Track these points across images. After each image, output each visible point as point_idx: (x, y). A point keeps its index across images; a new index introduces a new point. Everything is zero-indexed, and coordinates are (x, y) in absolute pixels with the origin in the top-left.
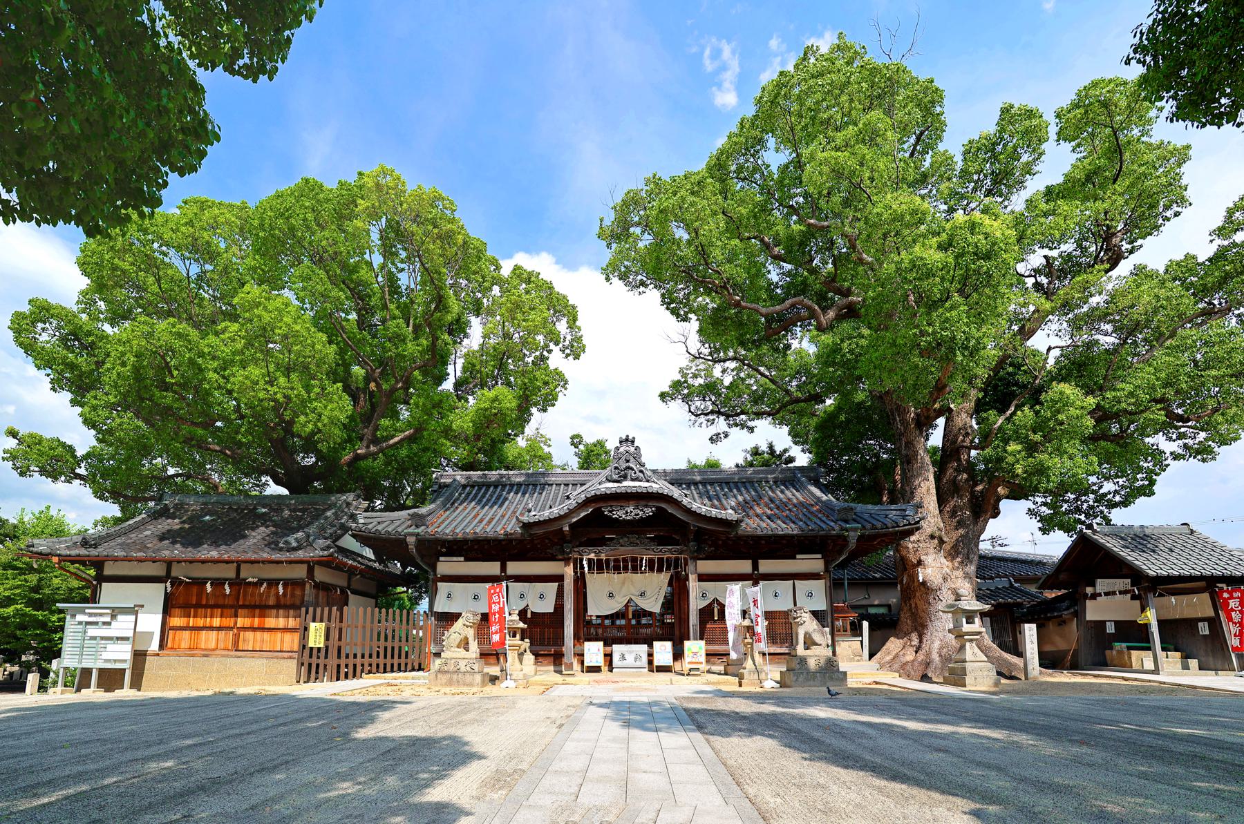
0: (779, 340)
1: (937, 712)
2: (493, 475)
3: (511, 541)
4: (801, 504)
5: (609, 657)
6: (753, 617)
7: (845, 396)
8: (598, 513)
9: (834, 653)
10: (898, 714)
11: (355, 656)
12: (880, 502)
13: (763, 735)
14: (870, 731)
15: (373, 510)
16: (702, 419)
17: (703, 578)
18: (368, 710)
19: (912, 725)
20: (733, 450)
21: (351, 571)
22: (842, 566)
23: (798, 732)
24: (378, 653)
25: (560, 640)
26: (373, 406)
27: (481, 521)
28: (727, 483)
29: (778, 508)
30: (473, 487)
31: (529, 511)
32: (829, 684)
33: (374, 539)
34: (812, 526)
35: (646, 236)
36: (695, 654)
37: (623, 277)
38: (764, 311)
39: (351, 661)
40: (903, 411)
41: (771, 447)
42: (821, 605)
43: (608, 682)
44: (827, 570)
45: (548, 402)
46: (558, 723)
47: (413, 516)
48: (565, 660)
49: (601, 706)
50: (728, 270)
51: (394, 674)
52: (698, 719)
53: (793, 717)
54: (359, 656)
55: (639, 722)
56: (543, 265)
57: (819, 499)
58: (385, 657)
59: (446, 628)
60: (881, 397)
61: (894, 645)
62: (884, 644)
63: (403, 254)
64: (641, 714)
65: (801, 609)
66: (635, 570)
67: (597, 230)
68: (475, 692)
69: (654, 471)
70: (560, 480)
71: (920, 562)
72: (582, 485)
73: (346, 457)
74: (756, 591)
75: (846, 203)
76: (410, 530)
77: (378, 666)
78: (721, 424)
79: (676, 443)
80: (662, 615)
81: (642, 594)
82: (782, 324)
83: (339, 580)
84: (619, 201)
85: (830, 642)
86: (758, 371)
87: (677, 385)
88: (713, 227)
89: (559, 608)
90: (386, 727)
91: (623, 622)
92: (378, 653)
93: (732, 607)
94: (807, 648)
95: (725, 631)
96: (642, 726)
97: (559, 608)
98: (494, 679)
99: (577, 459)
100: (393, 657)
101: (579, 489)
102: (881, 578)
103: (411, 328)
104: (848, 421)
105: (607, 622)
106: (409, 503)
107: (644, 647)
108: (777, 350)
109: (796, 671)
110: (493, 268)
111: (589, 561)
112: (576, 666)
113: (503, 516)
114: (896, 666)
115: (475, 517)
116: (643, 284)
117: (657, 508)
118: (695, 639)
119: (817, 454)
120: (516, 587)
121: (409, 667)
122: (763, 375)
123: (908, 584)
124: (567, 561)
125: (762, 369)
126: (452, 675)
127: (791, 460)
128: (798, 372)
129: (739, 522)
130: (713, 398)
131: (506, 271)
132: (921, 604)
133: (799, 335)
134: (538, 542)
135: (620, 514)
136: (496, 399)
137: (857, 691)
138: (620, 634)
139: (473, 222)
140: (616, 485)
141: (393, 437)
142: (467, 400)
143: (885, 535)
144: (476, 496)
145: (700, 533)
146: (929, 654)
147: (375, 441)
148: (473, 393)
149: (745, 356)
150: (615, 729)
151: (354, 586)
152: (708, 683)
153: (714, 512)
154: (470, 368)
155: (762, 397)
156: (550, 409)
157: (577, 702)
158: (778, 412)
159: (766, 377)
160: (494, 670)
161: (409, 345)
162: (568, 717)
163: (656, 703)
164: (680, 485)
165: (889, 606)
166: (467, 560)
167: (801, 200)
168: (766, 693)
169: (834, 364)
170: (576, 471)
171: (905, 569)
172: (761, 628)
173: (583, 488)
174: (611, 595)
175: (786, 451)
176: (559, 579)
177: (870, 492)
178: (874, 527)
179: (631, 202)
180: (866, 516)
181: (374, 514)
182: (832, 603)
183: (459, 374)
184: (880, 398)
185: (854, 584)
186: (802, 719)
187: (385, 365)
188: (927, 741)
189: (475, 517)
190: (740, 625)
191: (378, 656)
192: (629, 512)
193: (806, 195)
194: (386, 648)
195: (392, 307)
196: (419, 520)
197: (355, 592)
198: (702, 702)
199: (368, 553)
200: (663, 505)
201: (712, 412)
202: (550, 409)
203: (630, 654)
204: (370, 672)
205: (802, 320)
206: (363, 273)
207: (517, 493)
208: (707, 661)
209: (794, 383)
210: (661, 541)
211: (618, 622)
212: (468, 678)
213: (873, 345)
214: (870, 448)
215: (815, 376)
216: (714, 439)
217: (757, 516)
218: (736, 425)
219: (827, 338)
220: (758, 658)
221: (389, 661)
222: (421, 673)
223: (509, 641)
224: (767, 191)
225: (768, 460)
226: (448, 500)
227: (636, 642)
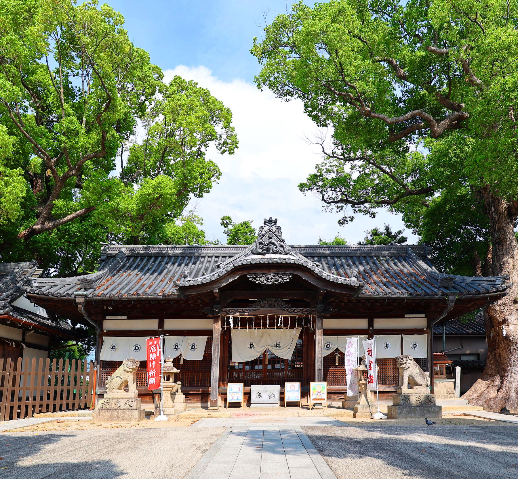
0: (400, 144)
1: (512, 437)
2: (154, 249)
3: (168, 301)
4: (411, 274)
5: (248, 395)
6: (367, 363)
7: (451, 190)
8: (244, 279)
9: (432, 392)
10: (481, 438)
11: (27, 399)
12: (474, 274)
13: (371, 456)
14: (458, 452)
15: (48, 276)
16: (333, 206)
17: (327, 332)
18: (33, 444)
19: (492, 447)
20: (358, 230)
21: (25, 328)
22: (442, 323)
23: (400, 453)
24: (49, 395)
25: (207, 382)
26: (49, 189)
27: (143, 285)
28: (351, 257)
29: (392, 277)
30: (136, 257)
31: (185, 277)
32: (427, 415)
33: (48, 300)
34: (419, 291)
35: (294, 55)
36: (319, 392)
37: (272, 86)
38: (389, 120)
39: (23, 403)
40: (496, 202)
41: (388, 229)
42: (423, 353)
43: (246, 415)
44: (429, 326)
45: (203, 190)
46: (203, 449)
47: (82, 281)
48: (211, 398)
49: (239, 434)
50: (360, 86)
51: (63, 413)
52: (320, 444)
53: (397, 442)
54: (31, 398)
55: (271, 447)
56: (201, 77)
57: (425, 271)
58: (55, 398)
59: (110, 374)
60: (480, 192)
61: (480, 385)
62: (472, 384)
63: (78, 61)
64: (273, 440)
65: (407, 357)
66: (272, 326)
67: (251, 47)
68: (133, 424)
69: (292, 247)
70: (210, 252)
71: (504, 321)
72: (230, 257)
73: (23, 231)
74: (371, 343)
75: (463, 35)
76: (80, 292)
77: (48, 406)
78: (348, 210)
79: (311, 225)
80: (293, 361)
81: (277, 345)
82: (403, 132)
83: (14, 335)
84: (270, 23)
85: (429, 383)
86: (380, 168)
87: (314, 179)
88: (349, 49)
89: (208, 356)
90: (48, 456)
91: (261, 367)
92: (49, 395)
93: (351, 355)
94: (410, 388)
95: (344, 375)
96: (273, 450)
97: (208, 356)
98: (149, 415)
99: (226, 236)
100: (62, 398)
101: (228, 260)
102: (473, 333)
103: (83, 126)
104: (452, 210)
105: (247, 367)
106: (80, 270)
107: (277, 387)
108: (398, 152)
109: (401, 405)
110: (156, 76)
111: (235, 318)
112: (220, 403)
113: (162, 281)
114: (481, 401)
115: (138, 282)
116: (289, 93)
117: (293, 275)
118: (319, 380)
119: (426, 236)
120: (172, 340)
121: (76, 406)
122: (384, 171)
123: (494, 337)
124: (215, 319)
125: (384, 167)
126: (114, 412)
127: (404, 240)
128: (414, 170)
129: (360, 287)
130: (343, 190)
131: (167, 80)
132: (504, 354)
133: (416, 140)
134: (192, 303)
135: (262, 280)
136: (159, 185)
137: (450, 421)
138: (257, 377)
139: (138, 36)
140: (260, 257)
141: (65, 215)
142: (132, 186)
143: (478, 299)
144: (138, 265)
145: (328, 295)
146: (508, 393)
147: (50, 218)
148: (137, 182)
149: (371, 156)
150: (251, 453)
151: (28, 339)
152: (329, 415)
153: (341, 280)
154: (134, 160)
155: (382, 190)
156: (205, 195)
157: (220, 432)
158: (395, 201)
159: (387, 173)
160: (150, 407)
161: (82, 139)
162: (211, 444)
163: (285, 432)
164: (313, 257)
165: (478, 355)
166: (129, 318)
167: (425, 31)
168: (376, 423)
169: (444, 165)
170: (226, 246)
171: (493, 326)
172: (374, 371)
173: (231, 259)
174: (251, 346)
175: (400, 232)
176: (209, 333)
177: (466, 266)
178: (469, 293)
179: (281, 26)
180: (463, 285)
181: (47, 280)
182: (432, 352)
183: (125, 164)
184: (480, 192)
185: (451, 338)
186: (404, 443)
187: (61, 154)
188: (503, 459)
189: (138, 282)
190: (357, 370)
191: (48, 398)
192: (271, 279)
193: (430, 27)
194: (55, 392)
195: (66, 106)
196: (88, 284)
197: (29, 345)
198: (323, 431)
199: (42, 312)
200: (299, 274)
201: (342, 200)
202: (205, 195)
203: (265, 393)
204: (40, 412)
205: (419, 128)
206: (40, 76)
207: (174, 263)
208: (329, 398)
209: (410, 179)
210: (294, 303)
211: (256, 367)
212: (127, 414)
213: (477, 149)
214: (468, 231)
215: (427, 173)
216: (342, 222)
217: (375, 283)
218: (361, 211)
219: (439, 144)
220: (370, 395)
221: (58, 402)
222: (87, 411)
223: (163, 383)
224: (396, 23)
225: (388, 239)
226: (115, 267)
227: (271, 383)
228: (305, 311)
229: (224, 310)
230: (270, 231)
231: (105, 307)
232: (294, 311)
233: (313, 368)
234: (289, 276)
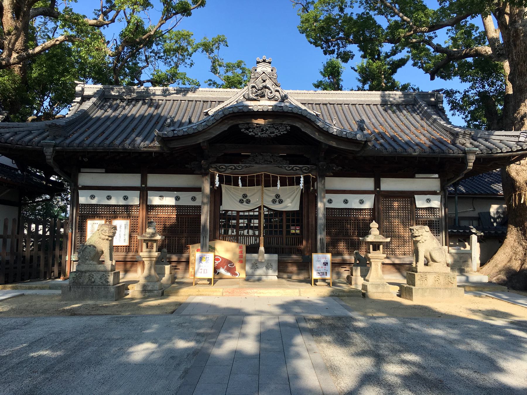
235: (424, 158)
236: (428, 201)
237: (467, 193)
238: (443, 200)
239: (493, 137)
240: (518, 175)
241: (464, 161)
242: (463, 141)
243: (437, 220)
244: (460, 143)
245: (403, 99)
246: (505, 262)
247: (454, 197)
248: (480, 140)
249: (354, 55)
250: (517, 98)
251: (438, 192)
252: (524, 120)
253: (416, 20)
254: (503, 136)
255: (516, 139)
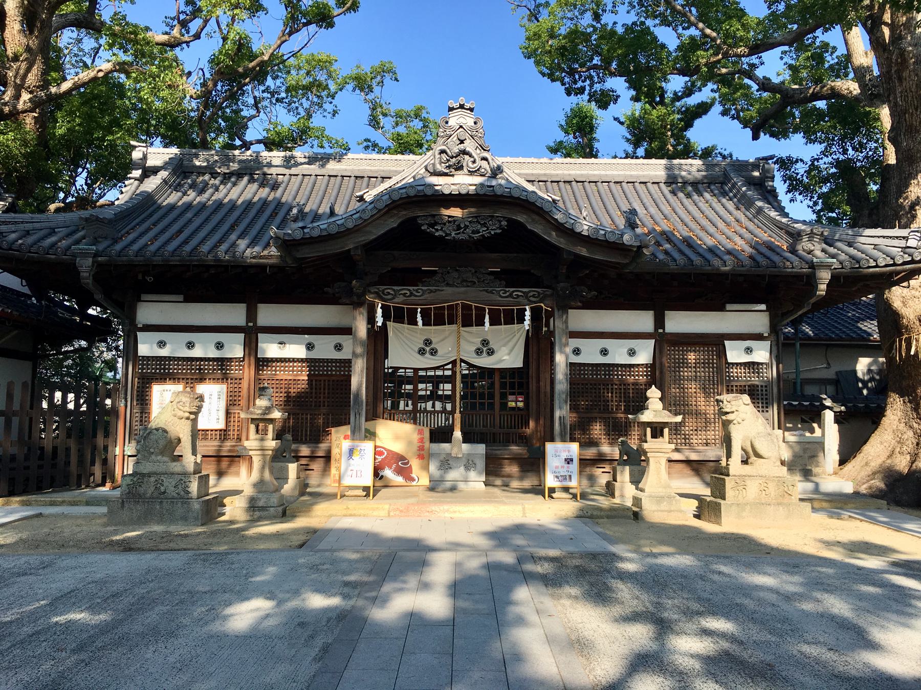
117: (509, 220)
166: (186, 300)
200: (521, 218)
228: (533, 296)
229: (373, 289)
230: (461, 127)
231: (140, 277)
232: (511, 295)
233: (548, 410)
234: (500, 221)
235: (741, 275)
236: (749, 350)
237: (817, 337)
238: (774, 348)
239: (862, 239)
240: (905, 305)
241: (810, 281)
242: (809, 246)
243: (764, 384)
244: (804, 250)
245: (704, 173)
246: (883, 458)
247: (794, 345)
248: (839, 244)
249: (618, 96)
250: (904, 172)
251: (766, 335)
252: (915, 210)
253: (727, 36)
254: (879, 237)
255: (902, 243)
